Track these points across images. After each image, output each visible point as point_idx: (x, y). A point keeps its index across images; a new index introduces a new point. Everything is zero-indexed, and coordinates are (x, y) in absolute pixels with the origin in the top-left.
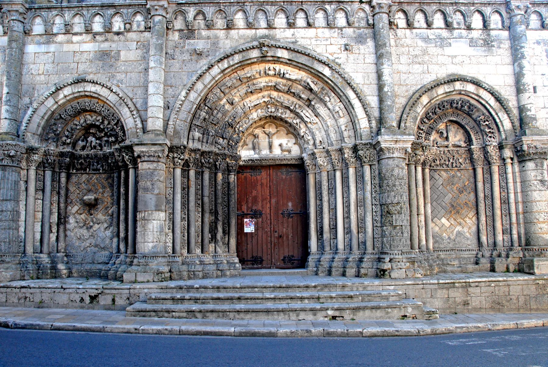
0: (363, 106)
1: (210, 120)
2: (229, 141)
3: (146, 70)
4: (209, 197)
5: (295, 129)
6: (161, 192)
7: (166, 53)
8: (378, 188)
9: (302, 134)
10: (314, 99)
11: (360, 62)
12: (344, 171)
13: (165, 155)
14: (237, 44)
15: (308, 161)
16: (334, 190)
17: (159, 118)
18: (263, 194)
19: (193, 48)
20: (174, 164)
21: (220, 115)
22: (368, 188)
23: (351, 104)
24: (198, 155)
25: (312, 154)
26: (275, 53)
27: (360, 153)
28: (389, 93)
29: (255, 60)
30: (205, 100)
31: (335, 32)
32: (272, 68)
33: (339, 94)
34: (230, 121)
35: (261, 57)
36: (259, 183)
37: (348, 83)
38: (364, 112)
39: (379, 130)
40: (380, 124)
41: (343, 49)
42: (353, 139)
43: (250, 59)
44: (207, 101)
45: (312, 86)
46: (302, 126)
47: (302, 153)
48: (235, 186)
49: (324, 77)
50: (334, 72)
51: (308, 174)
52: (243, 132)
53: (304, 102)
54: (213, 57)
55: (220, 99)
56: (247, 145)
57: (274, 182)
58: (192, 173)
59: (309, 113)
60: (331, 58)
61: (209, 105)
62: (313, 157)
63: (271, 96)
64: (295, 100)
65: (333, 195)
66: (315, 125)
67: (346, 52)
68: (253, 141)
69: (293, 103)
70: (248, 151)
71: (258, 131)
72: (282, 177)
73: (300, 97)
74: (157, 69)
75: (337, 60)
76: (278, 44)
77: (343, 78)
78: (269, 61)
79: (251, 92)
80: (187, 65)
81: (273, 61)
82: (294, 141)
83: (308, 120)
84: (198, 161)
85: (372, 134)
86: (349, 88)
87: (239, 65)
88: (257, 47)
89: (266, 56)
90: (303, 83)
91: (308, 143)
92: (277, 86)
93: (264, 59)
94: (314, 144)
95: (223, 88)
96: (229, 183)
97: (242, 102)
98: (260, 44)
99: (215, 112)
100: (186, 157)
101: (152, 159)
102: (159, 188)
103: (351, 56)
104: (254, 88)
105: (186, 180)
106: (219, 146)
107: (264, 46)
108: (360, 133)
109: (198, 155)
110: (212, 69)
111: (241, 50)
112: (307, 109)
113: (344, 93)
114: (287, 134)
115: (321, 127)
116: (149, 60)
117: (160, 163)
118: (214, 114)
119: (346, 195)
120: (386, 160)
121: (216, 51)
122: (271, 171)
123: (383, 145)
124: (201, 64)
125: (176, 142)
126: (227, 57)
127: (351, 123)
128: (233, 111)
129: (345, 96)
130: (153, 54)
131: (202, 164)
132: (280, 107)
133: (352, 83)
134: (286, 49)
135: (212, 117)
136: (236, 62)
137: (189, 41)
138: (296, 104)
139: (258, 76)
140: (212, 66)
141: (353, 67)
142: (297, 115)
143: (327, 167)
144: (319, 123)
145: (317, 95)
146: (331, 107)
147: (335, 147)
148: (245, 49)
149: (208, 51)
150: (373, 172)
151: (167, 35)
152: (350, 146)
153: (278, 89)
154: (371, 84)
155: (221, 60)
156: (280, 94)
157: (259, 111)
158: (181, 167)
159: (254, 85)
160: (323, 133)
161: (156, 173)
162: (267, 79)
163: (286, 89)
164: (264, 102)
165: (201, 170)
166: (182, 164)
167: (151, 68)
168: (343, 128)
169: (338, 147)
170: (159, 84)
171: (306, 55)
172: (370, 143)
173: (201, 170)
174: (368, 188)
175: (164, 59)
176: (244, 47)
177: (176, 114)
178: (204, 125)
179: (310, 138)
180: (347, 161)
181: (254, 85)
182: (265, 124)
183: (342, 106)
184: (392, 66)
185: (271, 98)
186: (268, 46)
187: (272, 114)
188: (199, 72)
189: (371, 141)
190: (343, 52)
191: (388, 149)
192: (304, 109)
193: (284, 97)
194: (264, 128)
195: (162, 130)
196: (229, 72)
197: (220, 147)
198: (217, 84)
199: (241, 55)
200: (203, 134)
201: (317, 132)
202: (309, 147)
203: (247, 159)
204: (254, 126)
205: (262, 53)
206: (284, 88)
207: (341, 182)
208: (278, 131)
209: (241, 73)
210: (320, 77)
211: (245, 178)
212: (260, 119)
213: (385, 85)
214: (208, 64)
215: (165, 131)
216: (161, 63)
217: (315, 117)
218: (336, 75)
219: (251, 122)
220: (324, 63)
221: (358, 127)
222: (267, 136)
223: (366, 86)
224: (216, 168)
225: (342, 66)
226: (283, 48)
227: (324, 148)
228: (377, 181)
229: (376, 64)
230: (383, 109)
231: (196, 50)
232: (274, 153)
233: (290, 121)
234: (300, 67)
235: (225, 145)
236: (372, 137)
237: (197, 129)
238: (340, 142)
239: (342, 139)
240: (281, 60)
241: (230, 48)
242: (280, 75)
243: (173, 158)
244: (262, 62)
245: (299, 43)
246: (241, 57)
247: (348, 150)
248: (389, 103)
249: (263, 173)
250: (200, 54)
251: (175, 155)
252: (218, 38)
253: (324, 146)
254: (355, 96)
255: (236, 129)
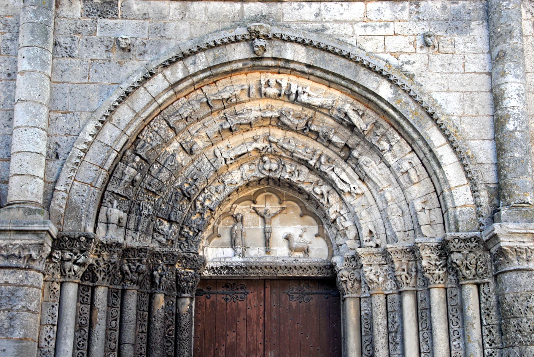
0: (461, 160)
1: (145, 184)
2: (182, 228)
3: (11, 75)
4: (134, 345)
5: (318, 207)
6: (30, 335)
7: (55, 44)
8: (496, 335)
9: (333, 217)
10: (358, 145)
11: (455, 70)
12: (421, 296)
13: (45, 255)
14: (203, 32)
15: (345, 273)
16: (398, 336)
17: (35, 177)
18: (250, 339)
19: (113, 35)
20: (63, 274)
21: (165, 174)
22: (475, 333)
23: (434, 156)
24: (115, 256)
25: (353, 257)
26: (279, 51)
27: (456, 257)
28: (517, 134)
29: (240, 65)
30: (135, 144)
31: (403, 9)
32: (273, 82)
33: (409, 136)
34: (186, 186)
35: (252, 59)
36: (243, 316)
37: (428, 114)
38: (463, 174)
39: (496, 210)
40: (499, 199)
41: (419, 43)
42: (440, 228)
43: (230, 63)
44: (139, 146)
45: (355, 118)
46: (333, 199)
47: (332, 255)
48: (190, 322)
49: (379, 102)
50: (400, 92)
51: (344, 300)
52: (211, 210)
53: (337, 150)
54: (155, 56)
55: (167, 142)
56: (219, 236)
57: (274, 315)
58: (101, 293)
59: (348, 174)
60: (393, 61)
61: (143, 154)
62: (354, 263)
63: (271, 138)
64: (319, 147)
65: (399, 347)
66: (359, 199)
67: (425, 50)
68: (232, 229)
69: (314, 152)
70: (220, 249)
71: (241, 209)
72: (290, 306)
73: (330, 141)
74: (35, 75)
75: (406, 67)
76: (287, 33)
77: (420, 103)
78: (268, 67)
79: (230, 129)
80: (99, 70)
81: (276, 67)
82: (315, 229)
83: (346, 188)
84: (115, 267)
85: (481, 219)
86: (430, 123)
87: (208, 73)
88: (244, 39)
89: (262, 58)
90: (335, 113)
91: (345, 235)
92: (283, 119)
93: (258, 63)
94: (358, 237)
95: (172, 121)
96: (178, 316)
97: (212, 149)
98: (250, 33)
99: (156, 167)
100: (91, 259)
101: (14, 263)
102: (25, 327)
103: (437, 59)
104: (236, 122)
105: (86, 309)
106: (161, 238)
107: (258, 38)
108: (455, 217)
109: (115, 256)
110: (152, 81)
111: (212, 44)
112: (344, 166)
113: (419, 135)
114: (301, 216)
115: (372, 201)
116: (16, 56)
117: (32, 272)
118: (153, 172)
119: (426, 347)
120: (514, 275)
121: (159, 44)
122: (268, 290)
123: (505, 243)
124: (130, 70)
125: (70, 227)
126: (183, 57)
127: (434, 196)
128: (192, 167)
129: (423, 139)
130: (26, 43)
131: (124, 273)
132: (288, 161)
133: (438, 114)
134: (303, 43)
135: (148, 178)
136: (201, 67)
137: (103, 20)
138: (320, 156)
139: (244, 97)
140: (152, 74)
141: (440, 81)
142: (323, 176)
143: (384, 286)
144: (368, 194)
145: (363, 138)
146: (392, 162)
147: (399, 246)
148: (219, 42)
149: (145, 44)
150: (484, 300)
151: (57, 6)
152: (434, 242)
153: (284, 124)
154: (477, 114)
155: (171, 62)
156: (289, 134)
157: (246, 167)
158: (78, 280)
159: (236, 114)
160: (377, 214)
161: (21, 293)
162: (263, 103)
163: (302, 124)
164: (257, 149)
165: (120, 287)
166: (80, 274)
167: (22, 73)
168: (418, 206)
169: (408, 244)
170: (38, 106)
171: (344, 57)
172: (475, 237)
173: (120, 287)
174: (475, 333)
175: (50, 56)
176: (217, 38)
177: (73, 170)
178: (131, 192)
179: (348, 224)
180: (426, 274)
181: (236, 114)
182: (257, 194)
183: (416, 161)
184: (524, 77)
185: (270, 142)
186: (266, 37)
187: (272, 175)
188: (125, 86)
189: (477, 234)
190: (418, 50)
191: (517, 251)
192: (337, 166)
193: (297, 141)
194: (255, 202)
195: (41, 201)
196: (186, 88)
197: (164, 240)
198: (160, 110)
199: (211, 53)
200: (129, 212)
201: (364, 214)
202: (347, 242)
203: (219, 265)
204: (235, 197)
205: (254, 52)
206: (296, 121)
207: (414, 318)
208: (283, 208)
209: (211, 91)
210: (370, 100)
211: (214, 304)
212: (247, 185)
213: (508, 116)
214: (144, 71)
215: (47, 205)
216: (44, 64)
217: (359, 183)
218: (405, 98)
219: (228, 190)
220: (380, 73)
221: (449, 204)
222: (260, 219)
223: (467, 120)
224: (153, 283)
225: (418, 79)
226: (296, 41)
227: (377, 246)
228: (494, 320)
229: (490, 74)
230: (503, 168)
231: (118, 41)
232: (273, 254)
233: (308, 188)
234: (330, 81)
235: (174, 237)
236: (481, 224)
237: (115, 202)
238: (411, 233)
239: (416, 229)
240: (292, 66)
241: (188, 39)
242: (289, 96)
243: (63, 260)
244: (253, 69)
245: (329, 32)
246: (211, 59)
247: (428, 252)
248: (517, 155)
249: (250, 296)
250: (127, 50)
251: (67, 256)
252: (165, 17)
253: (378, 242)
254: (443, 140)
255: (198, 203)
